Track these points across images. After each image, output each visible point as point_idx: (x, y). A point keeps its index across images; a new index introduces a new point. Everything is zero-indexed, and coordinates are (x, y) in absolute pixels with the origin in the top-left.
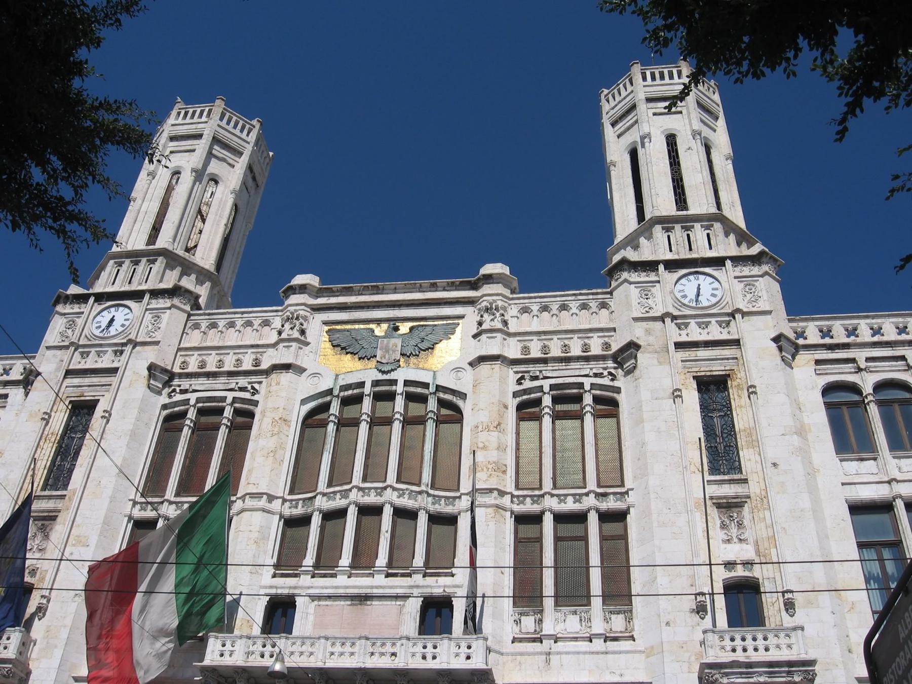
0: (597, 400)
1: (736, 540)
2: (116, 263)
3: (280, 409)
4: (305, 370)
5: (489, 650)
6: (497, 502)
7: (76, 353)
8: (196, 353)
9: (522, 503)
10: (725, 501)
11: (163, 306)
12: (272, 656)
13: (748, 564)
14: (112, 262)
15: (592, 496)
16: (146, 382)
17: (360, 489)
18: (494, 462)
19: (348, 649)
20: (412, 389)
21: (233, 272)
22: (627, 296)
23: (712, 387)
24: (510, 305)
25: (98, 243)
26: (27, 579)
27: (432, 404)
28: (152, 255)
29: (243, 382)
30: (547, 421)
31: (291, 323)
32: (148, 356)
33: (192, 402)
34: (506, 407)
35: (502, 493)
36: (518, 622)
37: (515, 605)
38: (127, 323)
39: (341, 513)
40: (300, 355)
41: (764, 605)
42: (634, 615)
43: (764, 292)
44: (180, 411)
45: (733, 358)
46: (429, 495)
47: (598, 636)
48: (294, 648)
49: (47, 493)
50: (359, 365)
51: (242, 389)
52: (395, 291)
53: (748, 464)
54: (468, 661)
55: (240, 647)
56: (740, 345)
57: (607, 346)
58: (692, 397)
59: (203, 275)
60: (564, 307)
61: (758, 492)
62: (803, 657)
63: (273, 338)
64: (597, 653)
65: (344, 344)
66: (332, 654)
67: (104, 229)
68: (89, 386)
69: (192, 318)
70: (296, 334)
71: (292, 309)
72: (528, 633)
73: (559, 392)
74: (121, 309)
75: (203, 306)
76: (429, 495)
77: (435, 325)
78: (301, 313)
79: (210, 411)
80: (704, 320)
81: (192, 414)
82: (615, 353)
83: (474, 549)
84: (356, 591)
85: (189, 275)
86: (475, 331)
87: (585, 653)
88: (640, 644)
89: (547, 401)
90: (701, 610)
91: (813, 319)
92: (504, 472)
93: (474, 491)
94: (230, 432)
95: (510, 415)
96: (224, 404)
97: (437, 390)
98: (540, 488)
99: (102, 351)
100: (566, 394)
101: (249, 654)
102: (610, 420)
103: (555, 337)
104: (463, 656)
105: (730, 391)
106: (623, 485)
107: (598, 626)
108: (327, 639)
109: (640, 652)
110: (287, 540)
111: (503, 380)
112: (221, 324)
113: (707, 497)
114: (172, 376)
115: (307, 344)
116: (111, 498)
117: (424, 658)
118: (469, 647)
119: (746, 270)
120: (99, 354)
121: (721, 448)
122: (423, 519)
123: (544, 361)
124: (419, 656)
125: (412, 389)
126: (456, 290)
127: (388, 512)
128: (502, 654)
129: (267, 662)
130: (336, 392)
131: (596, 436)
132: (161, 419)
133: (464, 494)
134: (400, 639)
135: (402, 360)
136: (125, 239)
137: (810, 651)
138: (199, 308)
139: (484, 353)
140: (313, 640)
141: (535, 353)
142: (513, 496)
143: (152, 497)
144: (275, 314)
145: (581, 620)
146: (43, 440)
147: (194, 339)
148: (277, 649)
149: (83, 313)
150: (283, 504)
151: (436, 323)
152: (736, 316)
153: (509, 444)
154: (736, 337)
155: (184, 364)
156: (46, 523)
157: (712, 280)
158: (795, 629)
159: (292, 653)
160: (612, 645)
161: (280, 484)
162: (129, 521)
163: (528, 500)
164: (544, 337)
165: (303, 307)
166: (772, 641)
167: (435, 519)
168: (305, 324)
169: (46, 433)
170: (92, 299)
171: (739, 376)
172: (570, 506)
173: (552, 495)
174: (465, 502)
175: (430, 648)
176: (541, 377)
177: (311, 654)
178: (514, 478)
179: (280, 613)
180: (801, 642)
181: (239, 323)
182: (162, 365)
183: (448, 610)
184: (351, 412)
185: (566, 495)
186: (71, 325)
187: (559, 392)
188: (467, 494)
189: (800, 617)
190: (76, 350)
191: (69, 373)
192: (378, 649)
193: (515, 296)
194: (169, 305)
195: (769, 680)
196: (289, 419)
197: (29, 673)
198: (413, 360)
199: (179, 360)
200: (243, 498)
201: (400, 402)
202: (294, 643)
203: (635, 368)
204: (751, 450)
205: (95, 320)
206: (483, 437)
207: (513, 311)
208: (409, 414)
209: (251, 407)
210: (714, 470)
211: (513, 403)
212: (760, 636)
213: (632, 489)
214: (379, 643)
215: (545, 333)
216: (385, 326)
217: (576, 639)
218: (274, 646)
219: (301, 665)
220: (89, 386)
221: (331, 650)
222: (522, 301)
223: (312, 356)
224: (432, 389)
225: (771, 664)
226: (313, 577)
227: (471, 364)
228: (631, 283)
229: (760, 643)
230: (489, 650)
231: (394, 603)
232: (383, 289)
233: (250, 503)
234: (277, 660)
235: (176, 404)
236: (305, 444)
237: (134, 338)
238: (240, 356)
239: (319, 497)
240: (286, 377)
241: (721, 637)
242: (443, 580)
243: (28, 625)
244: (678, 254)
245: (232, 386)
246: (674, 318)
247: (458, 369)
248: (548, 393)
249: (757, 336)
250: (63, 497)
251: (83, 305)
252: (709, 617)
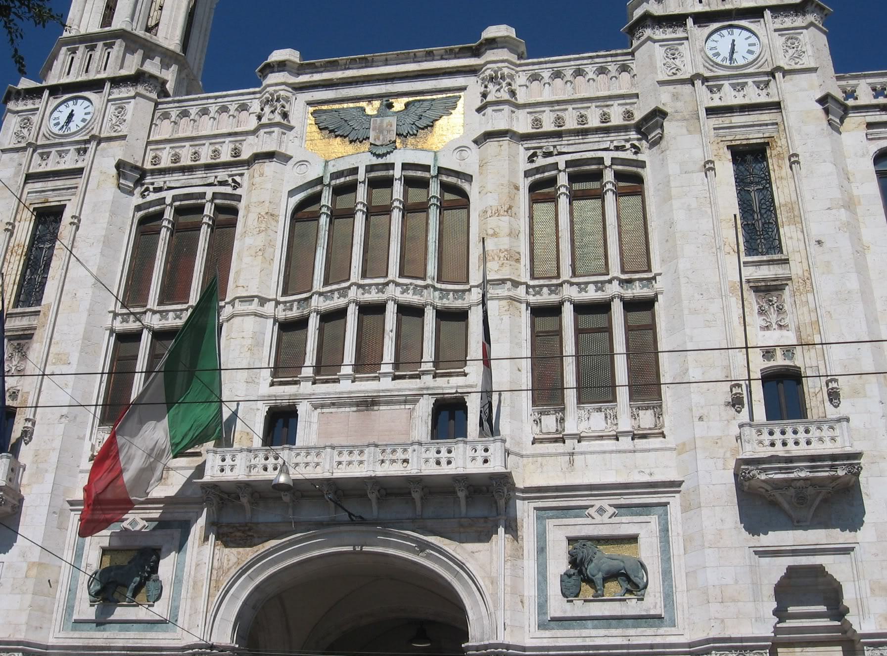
0: (618, 176)
1: (775, 326)
2: (69, 50)
3: (265, 202)
4: (291, 158)
5: (508, 452)
6: (510, 294)
7: (35, 155)
8: (168, 146)
9: (539, 293)
10: (763, 284)
11: (127, 95)
12: (275, 469)
13: (788, 350)
14: (64, 49)
15: (616, 283)
16: (115, 182)
17: (360, 286)
18: (506, 250)
19: (356, 457)
20: (411, 173)
21: (205, 35)
22: (651, 57)
23: (749, 157)
24: (517, 72)
25: (44, 26)
26: (9, 402)
27: (434, 189)
28: (109, 38)
29: (222, 175)
30: (563, 202)
31: (272, 106)
32: (113, 153)
33: (168, 201)
34: (517, 188)
35: (516, 284)
36: (538, 422)
37: (534, 403)
38: (88, 117)
39: (341, 313)
40: (285, 142)
41: (806, 395)
42: (664, 410)
43: (809, 47)
44: (155, 211)
45: (773, 124)
46: (435, 289)
47: (625, 433)
48: (299, 459)
49: (19, 310)
50: (350, 149)
51: (223, 183)
52: (386, 63)
53: (789, 242)
54: (486, 465)
55: (241, 461)
56: (780, 108)
57: (629, 115)
58: (726, 169)
59: (167, 57)
60: (579, 72)
61: (800, 273)
62: (848, 450)
63: (253, 123)
64: (625, 452)
65: (332, 127)
66: (340, 463)
67: (50, 10)
68: (53, 190)
69: (160, 106)
70: (278, 118)
71: (271, 89)
72: (549, 433)
73: (576, 169)
74: (80, 101)
75: (171, 93)
76: (435, 289)
77: (434, 100)
78: (282, 93)
79: (189, 210)
80: (740, 81)
81: (169, 214)
82: (638, 122)
83: (487, 345)
85: (152, 59)
86: (478, 104)
87: (611, 452)
88: (671, 441)
89: (563, 179)
90: (736, 402)
91: (865, 76)
92: (518, 260)
93: (485, 283)
94: (212, 231)
95: (522, 197)
96: (204, 201)
97: (439, 173)
98: (558, 276)
99: (63, 151)
100: (583, 171)
101: (250, 467)
102: (634, 198)
103: (570, 107)
104: (480, 460)
105: (770, 161)
106: (649, 270)
107: (625, 423)
108: (333, 447)
109: (670, 449)
110: (283, 345)
111: (513, 158)
112: (193, 111)
113: (744, 280)
114: (143, 173)
115: (291, 128)
116: (89, 311)
117: (438, 463)
118: (486, 450)
119: (788, 22)
120: (60, 154)
121: (759, 225)
122: (430, 316)
123: (558, 135)
124: (432, 462)
125: (411, 173)
126: (456, 58)
127: (391, 310)
128: (522, 456)
129: (271, 475)
130: (326, 181)
131: (618, 217)
132: (136, 221)
133: (474, 287)
134: (412, 444)
135: (398, 141)
136: (76, 22)
137: (855, 443)
138: (167, 95)
139: (490, 128)
140: (318, 450)
141: (548, 126)
142: (528, 287)
143: (133, 307)
144: (252, 96)
145: (606, 417)
146: (9, 253)
147: (164, 130)
148: (280, 461)
149: (37, 109)
150: (276, 307)
151: (434, 97)
152: (776, 75)
153: (522, 229)
154: (776, 99)
155: (156, 159)
156: (22, 342)
157: (749, 34)
158: (839, 420)
159: (297, 465)
160: (640, 443)
161: (272, 287)
162: (111, 335)
163: (545, 290)
164: (557, 108)
165: (283, 87)
166: (814, 433)
167: (443, 315)
168: (287, 106)
169: (11, 245)
170: (46, 93)
171: (779, 144)
172: (592, 294)
173: (572, 284)
174: (475, 295)
175: (444, 454)
176: (555, 152)
177: (318, 464)
178: (528, 266)
179: (281, 424)
180: (846, 433)
181: (213, 109)
182: (132, 161)
183: (462, 412)
184: (344, 201)
185: (587, 283)
186: (26, 123)
187: (576, 169)
188: (477, 286)
189: (845, 408)
190: (34, 151)
191: (30, 177)
192: (388, 456)
193: (523, 62)
194: (132, 93)
195: (811, 475)
196: (276, 214)
197: (21, 500)
198: (410, 140)
199: (150, 155)
200: (232, 303)
201: (398, 189)
202: (298, 454)
203: (661, 138)
204: (793, 227)
205: (52, 116)
206: (493, 222)
207: (521, 79)
208: (410, 201)
209: (234, 203)
210: (750, 251)
211: (524, 184)
212: (801, 429)
213: (660, 274)
214: (389, 450)
215: (558, 102)
216: (377, 103)
217: (601, 438)
218: (276, 458)
219: (308, 477)
220: (53, 190)
221: (338, 459)
222: (531, 67)
223: (297, 141)
224: (434, 172)
225: (813, 458)
226: (314, 383)
227: (476, 142)
228: (655, 41)
229: (802, 436)
230: (508, 452)
231: (403, 407)
232: (373, 61)
233: (240, 307)
234: (281, 471)
235: (538, 170)
236: (296, 241)
237: (97, 134)
238: (217, 146)
239: (315, 297)
240: (270, 167)
241: (759, 431)
242: (456, 381)
243: (15, 451)
244: (709, 5)
245: (211, 180)
246: (705, 80)
247: (461, 149)
248: (564, 171)
249: (801, 97)
250: (37, 313)
251: (37, 101)
252: (745, 410)
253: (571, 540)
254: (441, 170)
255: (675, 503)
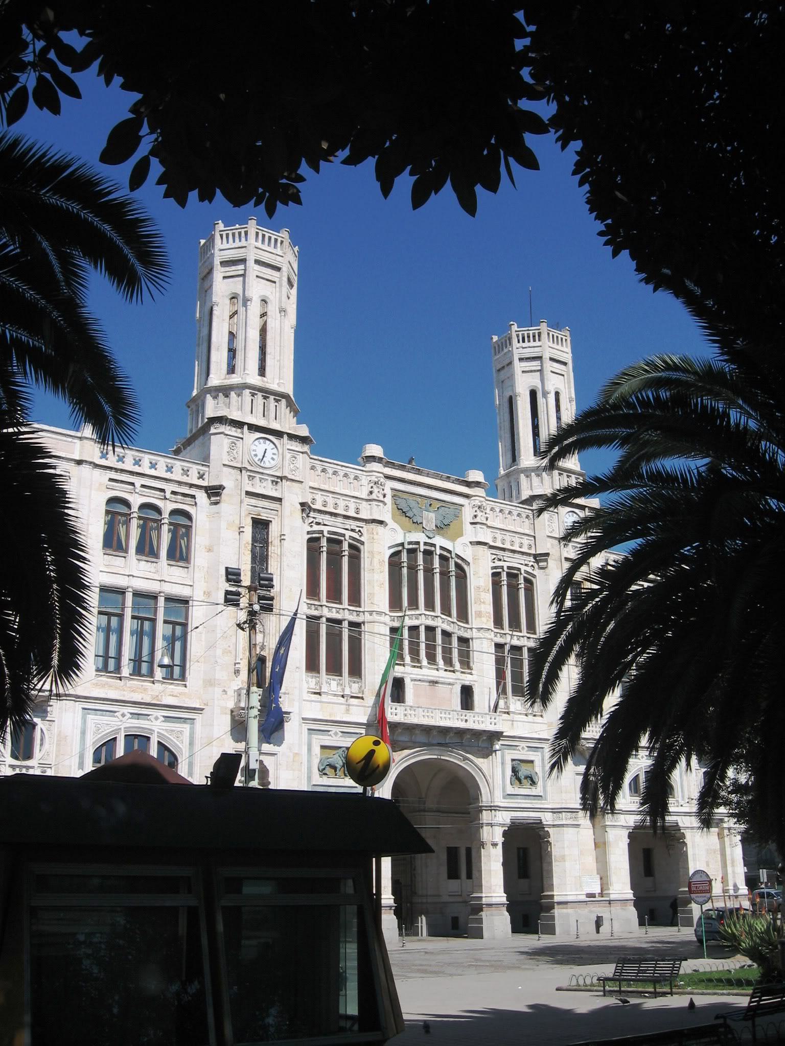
52: (428, 475)
58: (248, 530)
84: (432, 678)
114: (310, 509)
209: (359, 545)
235: (314, 532)
253: (513, 760)
254: (458, 556)
255: (198, 717)
